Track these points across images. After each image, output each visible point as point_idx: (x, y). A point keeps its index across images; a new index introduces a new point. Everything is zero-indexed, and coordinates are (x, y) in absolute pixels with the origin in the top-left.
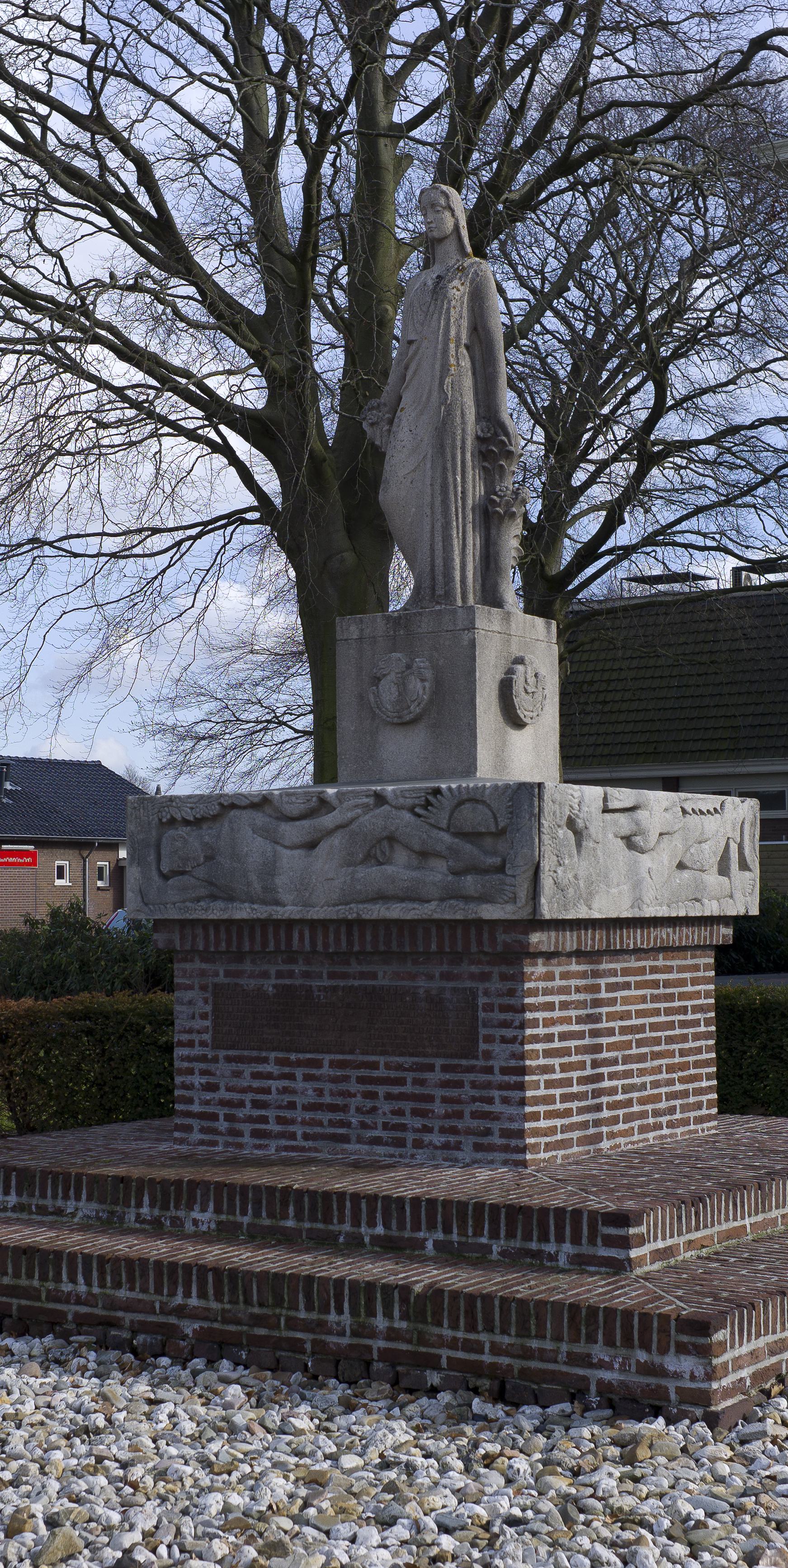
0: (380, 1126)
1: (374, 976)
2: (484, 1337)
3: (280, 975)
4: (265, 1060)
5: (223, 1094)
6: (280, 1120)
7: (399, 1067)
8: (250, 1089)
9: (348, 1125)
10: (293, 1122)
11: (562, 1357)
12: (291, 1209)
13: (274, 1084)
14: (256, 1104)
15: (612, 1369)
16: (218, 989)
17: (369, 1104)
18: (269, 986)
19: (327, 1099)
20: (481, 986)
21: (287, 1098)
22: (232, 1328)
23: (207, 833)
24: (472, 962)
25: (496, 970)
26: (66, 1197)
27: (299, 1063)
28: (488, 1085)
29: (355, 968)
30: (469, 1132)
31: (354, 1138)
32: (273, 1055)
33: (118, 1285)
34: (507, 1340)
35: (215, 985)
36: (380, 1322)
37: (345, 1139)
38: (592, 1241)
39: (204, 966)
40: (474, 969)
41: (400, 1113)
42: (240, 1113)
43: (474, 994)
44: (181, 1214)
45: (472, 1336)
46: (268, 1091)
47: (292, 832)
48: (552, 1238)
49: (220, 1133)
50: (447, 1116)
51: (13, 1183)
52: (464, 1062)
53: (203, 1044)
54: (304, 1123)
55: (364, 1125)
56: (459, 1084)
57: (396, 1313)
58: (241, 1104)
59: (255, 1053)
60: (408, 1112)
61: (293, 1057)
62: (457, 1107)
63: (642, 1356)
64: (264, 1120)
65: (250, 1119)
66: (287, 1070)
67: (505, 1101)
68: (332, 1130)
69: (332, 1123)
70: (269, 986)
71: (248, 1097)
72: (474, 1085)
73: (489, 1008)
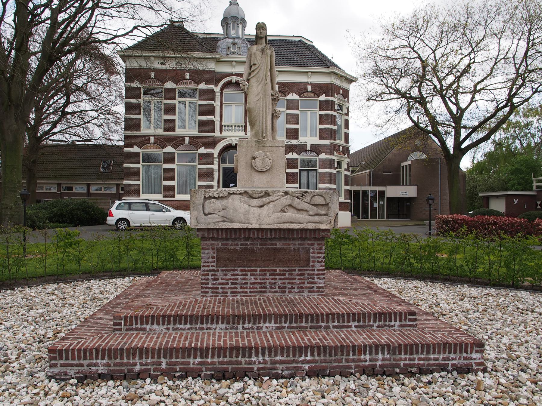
0: (277, 288)
1: (276, 245)
2: (415, 356)
3: (242, 244)
4: (237, 270)
5: (220, 281)
6: (241, 288)
7: (284, 270)
8: (231, 279)
9: (266, 288)
10: (246, 288)
11: (441, 358)
12: (304, 320)
13: (239, 277)
14: (232, 283)
15: (455, 359)
16: (218, 250)
17: (273, 281)
18: (238, 248)
19: (259, 281)
20: (311, 247)
21: (244, 281)
22: (324, 365)
23: (224, 202)
24: (308, 240)
25: (316, 242)
26: (212, 323)
27: (249, 271)
28: (313, 274)
29: (269, 242)
30: (307, 288)
31: (268, 292)
32: (239, 269)
33: (276, 355)
34: (422, 356)
35: (218, 248)
36: (380, 356)
37: (265, 292)
38: (405, 320)
39: (213, 242)
40: (309, 242)
41: (284, 283)
42: (227, 286)
43: (309, 249)
44: (261, 325)
45: (412, 357)
46: (237, 279)
47: (255, 202)
48: (393, 320)
49: (219, 293)
50: (300, 283)
51: (188, 320)
52: (305, 268)
53: (212, 266)
54: (250, 288)
55: (271, 288)
56: (304, 274)
57: (386, 353)
58: (227, 284)
59: (233, 268)
60: (286, 283)
61: (247, 269)
62: (303, 281)
63: (465, 355)
64: (236, 288)
65: (230, 288)
66: (244, 273)
67: (318, 278)
68: (260, 290)
69: (260, 288)
70: (238, 248)
71: (230, 282)
72: (308, 274)
73: (314, 253)
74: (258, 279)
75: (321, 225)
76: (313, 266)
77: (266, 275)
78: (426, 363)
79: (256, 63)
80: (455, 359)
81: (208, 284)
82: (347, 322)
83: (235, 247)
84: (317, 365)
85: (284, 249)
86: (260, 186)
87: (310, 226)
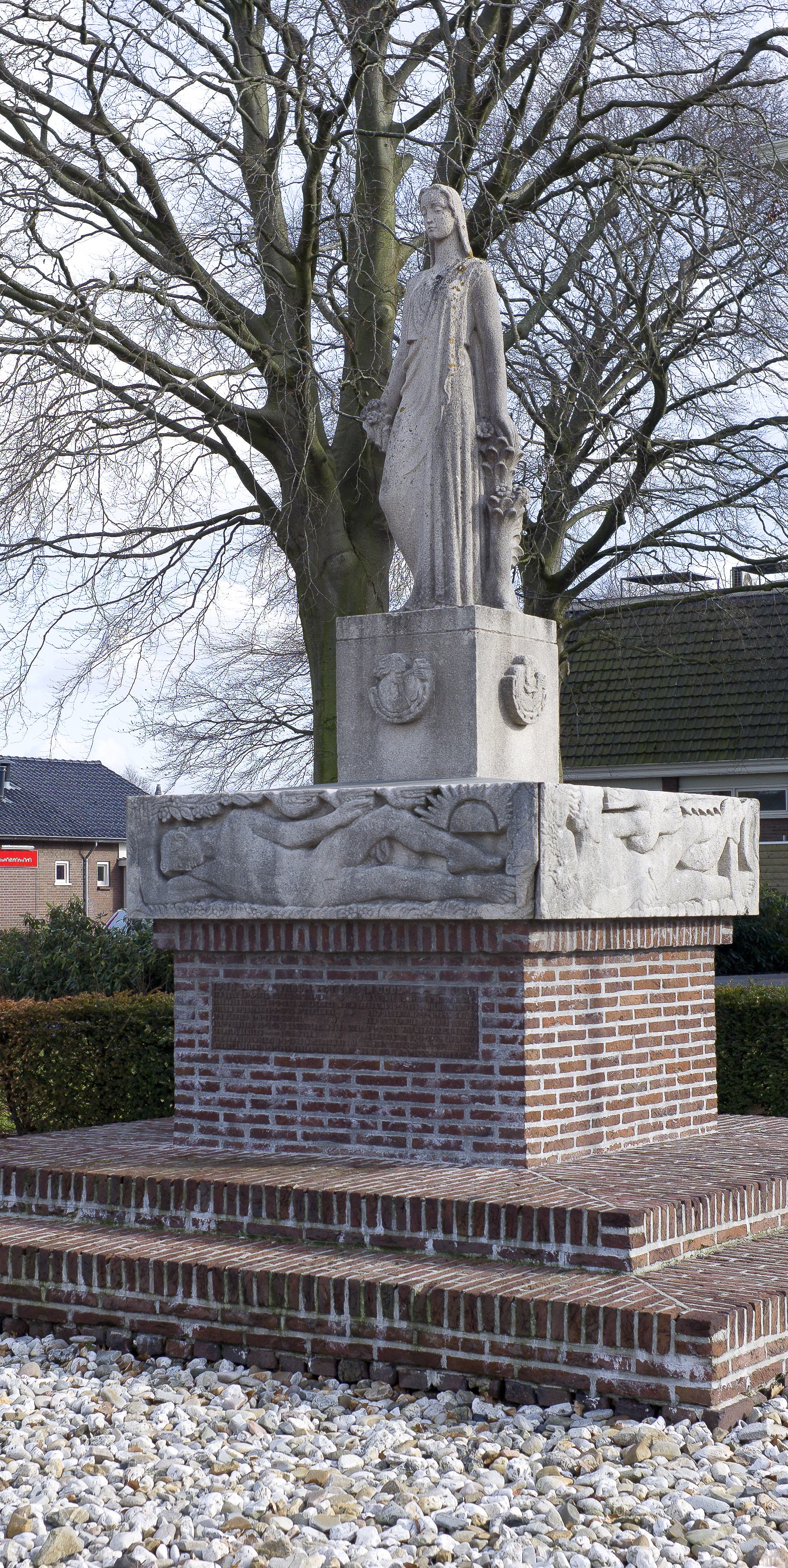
0: (380, 1126)
1: (374, 976)
2: (484, 1337)
3: (280, 975)
4: (265, 1060)
5: (223, 1094)
6: (280, 1120)
7: (399, 1067)
8: (250, 1089)
9: (348, 1125)
10: (293, 1122)
11: (562, 1357)
13: (274, 1084)
14: (256, 1104)
15: (612, 1368)
18: (269, 986)
19: (327, 1099)
20: (481, 986)
21: (287, 1098)
22: (232, 1328)
23: (207, 834)
24: (472, 962)
25: (496, 970)
26: (66, 1197)
27: (299, 1063)
28: (488, 1085)
29: (354, 968)
30: (469, 1132)
31: (354, 1138)
32: (273, 1055)
33: (118, 1285)
34: (506, 1340)
35: (215, 985)
36: (380, 1322)
37: (345, 1139)
38: (592, 1241)
39: (204, 966)
40: (474, 969)
41: (400, 1113)
42: (240, 1113)
43: (474, 994)
44: (181, 1214)
45: (472, 1336)
46: (268, 1091)
47: (292, 832)
48: (552, 1238)
49: (220, 1133)
50: (447, 1116)
52: (464, 1062)
53: (203, 1044)
54: (304, 1123)
55: (364, 1126)
56: (460, 1084)
57: (396, 1313)
58: (241, 1104)
59: (255, 1053)
60: (408, 1112)
61: (293, 1057)
62: (457, 1107)
63: (642, 1356)
64: (264, 1120)
65: (250, 1119)
66: (287, 1070)
67: (505, 1101)
68: (332, 1130)
69: (332, 1123)
70: (269, 986)
71: (248, 1097)
72: (474, 1085)
73: (489, 1008)
74: (326, 1093)
77: (346, 1079)
78: (517, 1364)
80: (612, 1368)
82: (412, 1230)
83: (260, 981)
84: (216, 1325)
85: (398, 994)
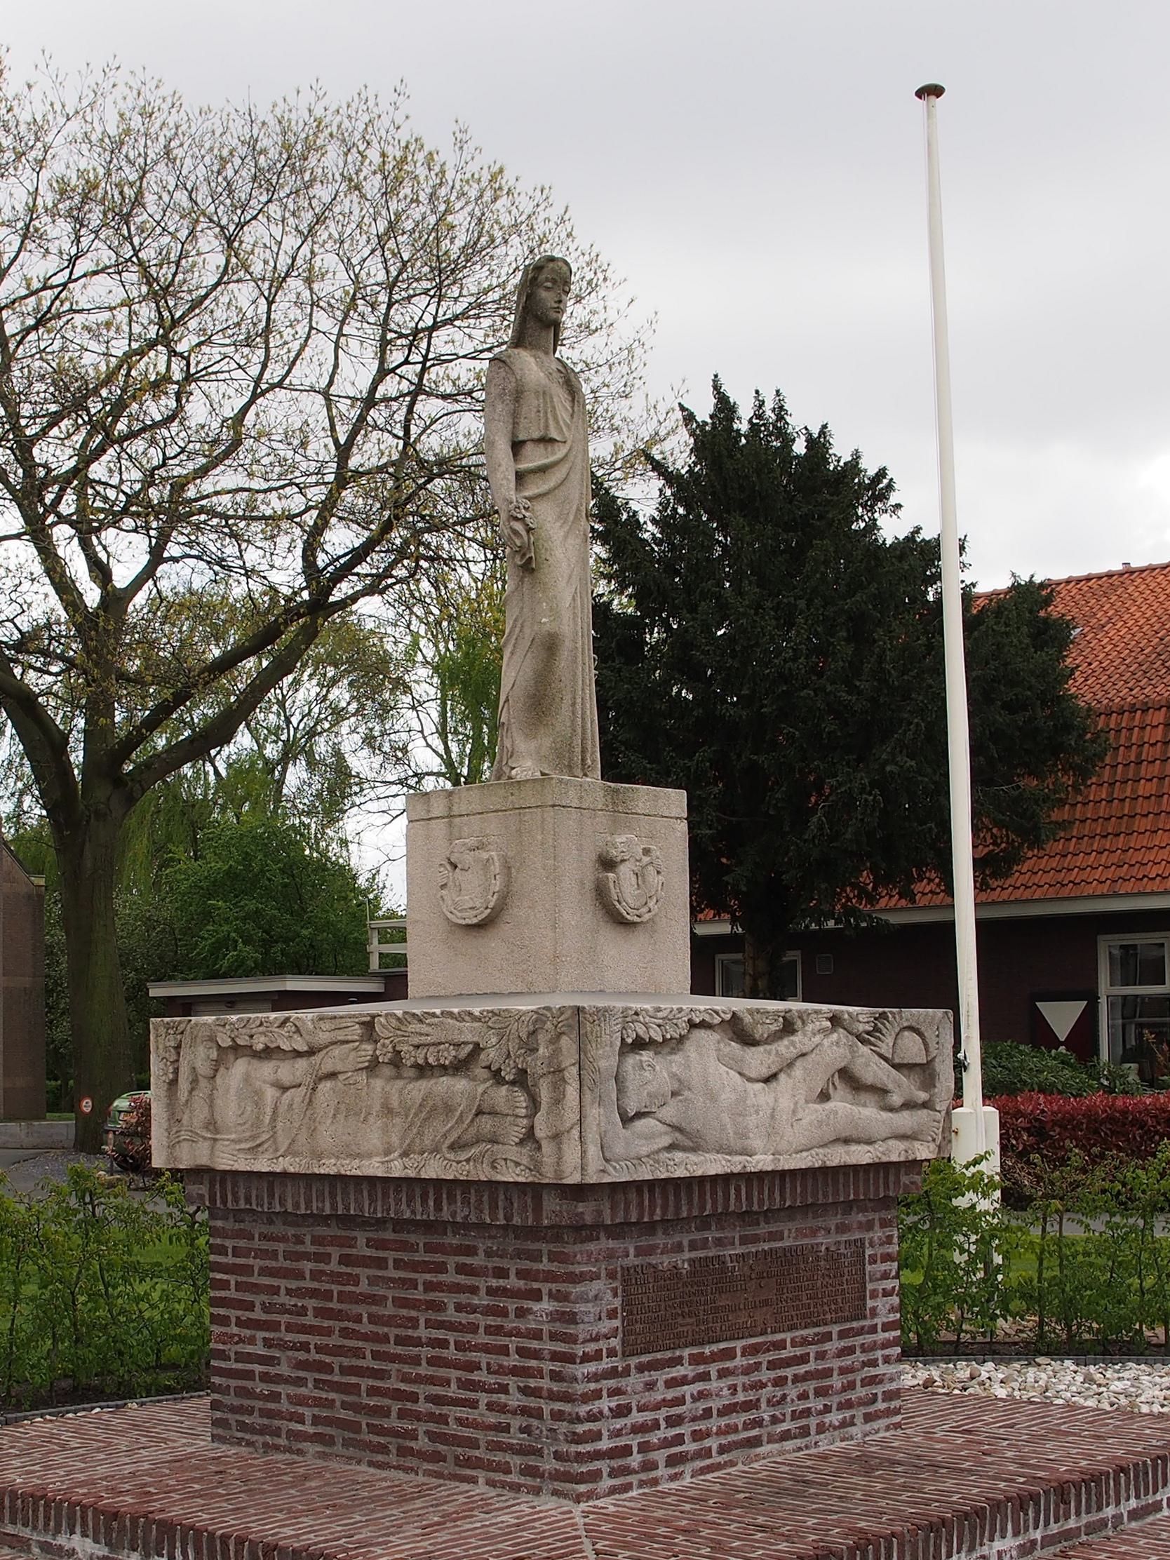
3: (693, 1246)
4: (678, 1361)
18: (683, 1260)
25: (877, 1216)
37: (754, 1442)
39: (612, 1244)
52: (855, 1324)
53: (612, 1353)
58: (656, 1425)
61: (707, 1350)
73: (873, 1260)
75: (917, 1144)
76: (873, 1310)
79: (554, 435)
81: (597, 1436)
86: (622, 985)
87: (895, 1152)
